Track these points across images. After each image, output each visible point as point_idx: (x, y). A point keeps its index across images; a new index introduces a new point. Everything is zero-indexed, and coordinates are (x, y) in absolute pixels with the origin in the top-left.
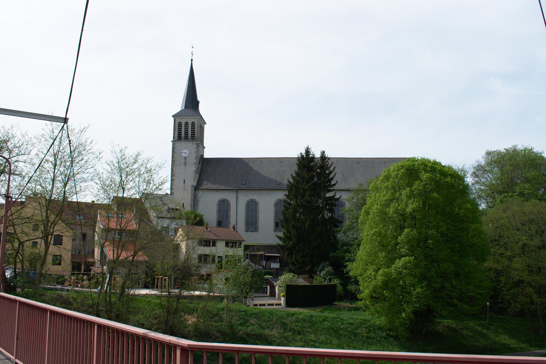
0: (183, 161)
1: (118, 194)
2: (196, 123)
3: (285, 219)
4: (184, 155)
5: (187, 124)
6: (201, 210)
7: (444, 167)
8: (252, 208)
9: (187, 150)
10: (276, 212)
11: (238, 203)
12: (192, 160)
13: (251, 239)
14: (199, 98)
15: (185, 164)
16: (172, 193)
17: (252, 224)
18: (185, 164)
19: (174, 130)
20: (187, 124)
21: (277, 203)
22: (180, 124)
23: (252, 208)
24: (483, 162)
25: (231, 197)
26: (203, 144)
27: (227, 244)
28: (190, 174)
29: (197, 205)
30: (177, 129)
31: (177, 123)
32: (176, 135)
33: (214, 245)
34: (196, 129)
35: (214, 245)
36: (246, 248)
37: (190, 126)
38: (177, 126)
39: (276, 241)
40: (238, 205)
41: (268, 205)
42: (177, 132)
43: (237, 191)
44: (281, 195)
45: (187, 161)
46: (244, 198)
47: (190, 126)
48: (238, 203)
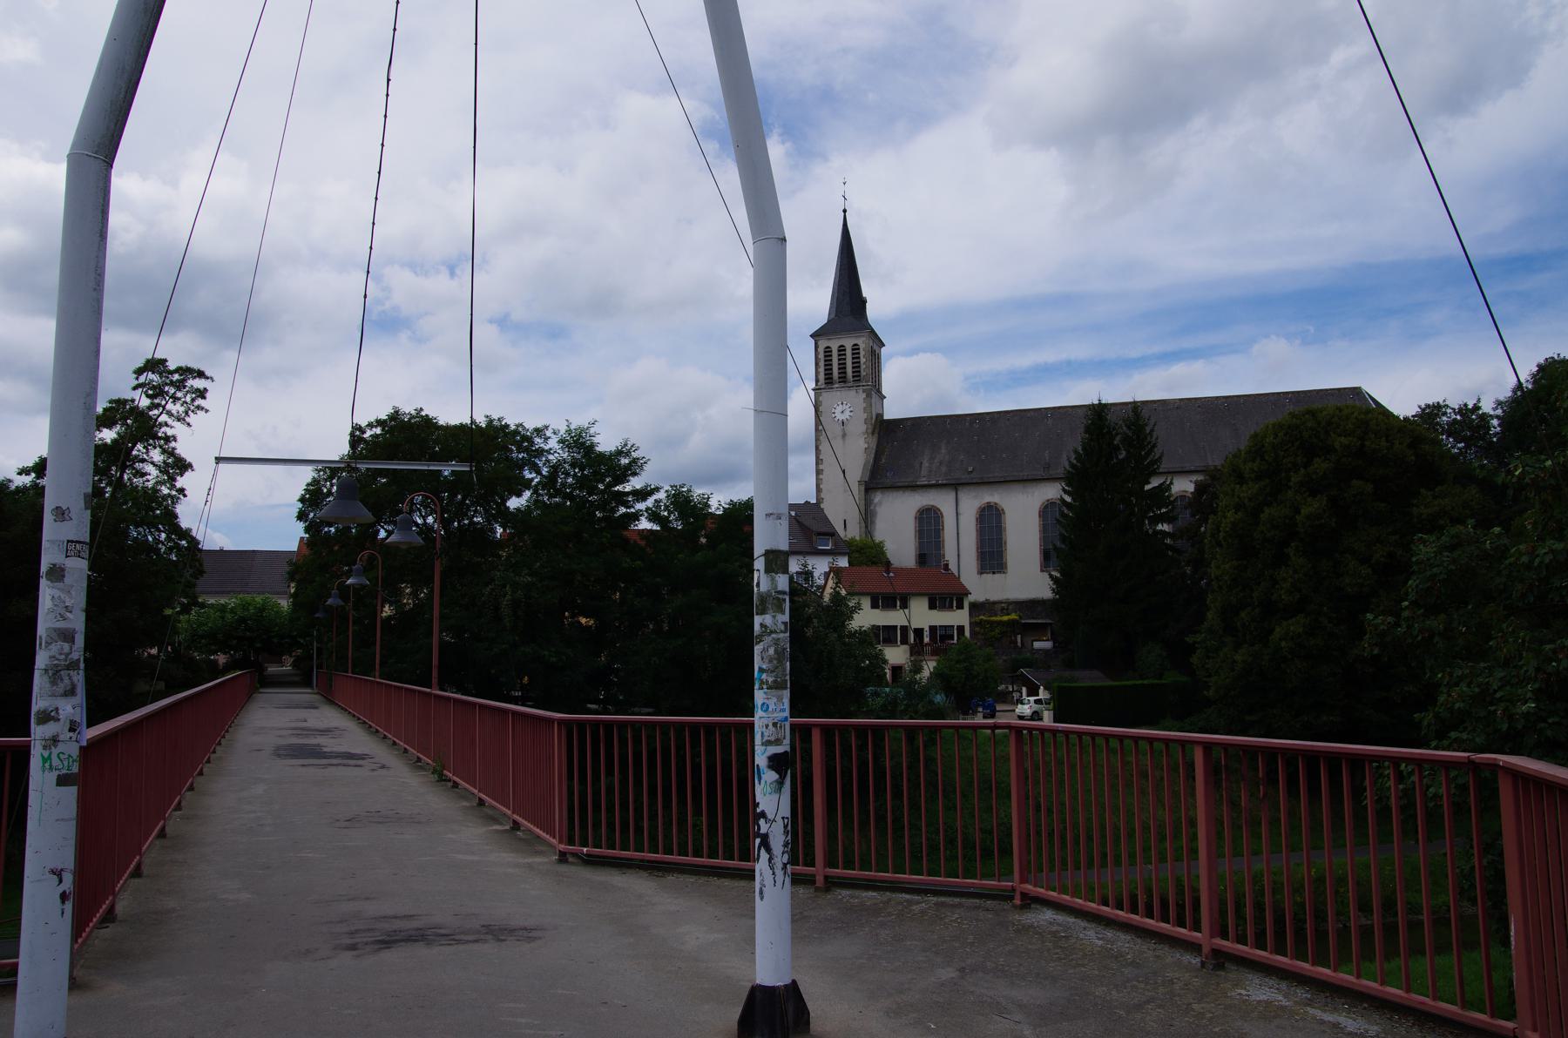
0: (839, 428)
1: (784, 593)
2: (862, 346)
3: (1067, 541)
4: (840, 417)
5: (842, 349)
6: (881, 533)
7: (1406, 419)
8: (991, 521)
9: (846, 407)
10: (1044, 529)
11: (960, 517)
12: (859, 428)
13: (981, 587)
14: (865, 293)
15: (844, 435)
16: (820, 500)
17: (992, 557)
18: (844, 435)
19: (817, 364)
20: (842, 349)
21: (1046, 510)
22: (828, 351)
23: (991, 521)
24: (1487, 407)
25: (943, 502)
26: (879, 391)
27: (932, 606)
28: (856, 453)
29: (873, 522)
30: (822, 363)
31: (821, 350)
32: (822, 377)
33: (905, 606)
34: (863, 360)
35: (905, 606)
36: (975, 607)
37: (849, 353)
38: (821, 356)
39: (1047, 594)
40: (961, 518)
41: (1024, 511)
42: (822, 370)
43: (955, 486)
44: (1052, 491)
45: (848, 428)
46: (971, 503)
47: (849, 353)
48: (960, 517)
